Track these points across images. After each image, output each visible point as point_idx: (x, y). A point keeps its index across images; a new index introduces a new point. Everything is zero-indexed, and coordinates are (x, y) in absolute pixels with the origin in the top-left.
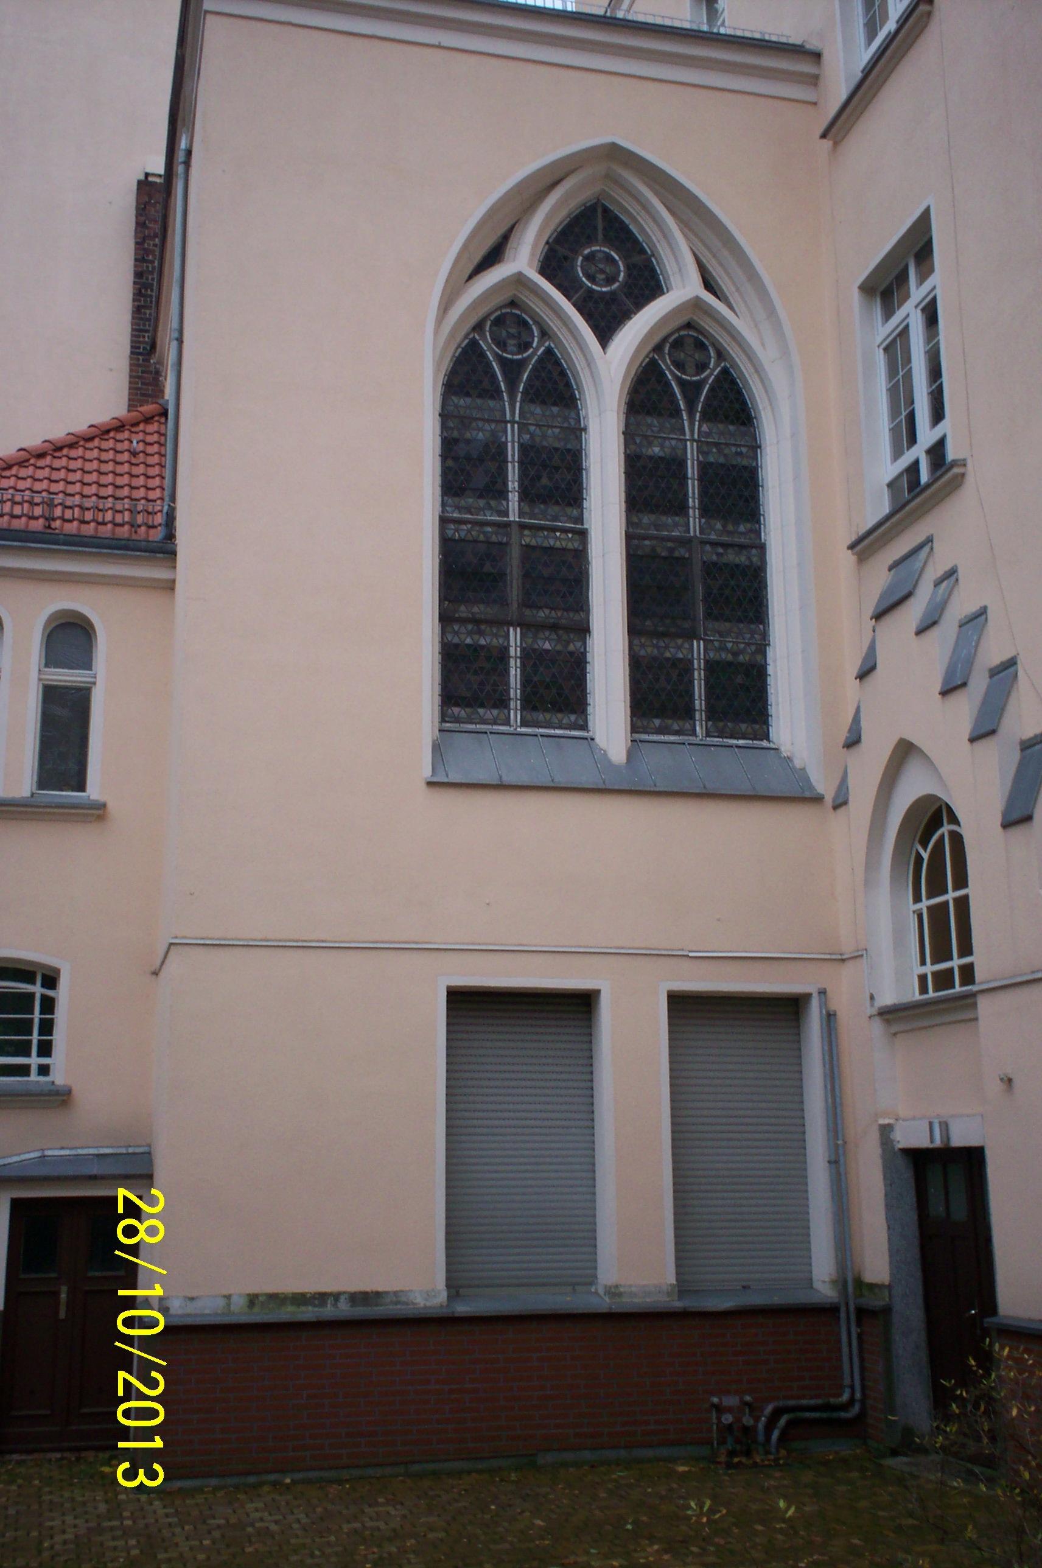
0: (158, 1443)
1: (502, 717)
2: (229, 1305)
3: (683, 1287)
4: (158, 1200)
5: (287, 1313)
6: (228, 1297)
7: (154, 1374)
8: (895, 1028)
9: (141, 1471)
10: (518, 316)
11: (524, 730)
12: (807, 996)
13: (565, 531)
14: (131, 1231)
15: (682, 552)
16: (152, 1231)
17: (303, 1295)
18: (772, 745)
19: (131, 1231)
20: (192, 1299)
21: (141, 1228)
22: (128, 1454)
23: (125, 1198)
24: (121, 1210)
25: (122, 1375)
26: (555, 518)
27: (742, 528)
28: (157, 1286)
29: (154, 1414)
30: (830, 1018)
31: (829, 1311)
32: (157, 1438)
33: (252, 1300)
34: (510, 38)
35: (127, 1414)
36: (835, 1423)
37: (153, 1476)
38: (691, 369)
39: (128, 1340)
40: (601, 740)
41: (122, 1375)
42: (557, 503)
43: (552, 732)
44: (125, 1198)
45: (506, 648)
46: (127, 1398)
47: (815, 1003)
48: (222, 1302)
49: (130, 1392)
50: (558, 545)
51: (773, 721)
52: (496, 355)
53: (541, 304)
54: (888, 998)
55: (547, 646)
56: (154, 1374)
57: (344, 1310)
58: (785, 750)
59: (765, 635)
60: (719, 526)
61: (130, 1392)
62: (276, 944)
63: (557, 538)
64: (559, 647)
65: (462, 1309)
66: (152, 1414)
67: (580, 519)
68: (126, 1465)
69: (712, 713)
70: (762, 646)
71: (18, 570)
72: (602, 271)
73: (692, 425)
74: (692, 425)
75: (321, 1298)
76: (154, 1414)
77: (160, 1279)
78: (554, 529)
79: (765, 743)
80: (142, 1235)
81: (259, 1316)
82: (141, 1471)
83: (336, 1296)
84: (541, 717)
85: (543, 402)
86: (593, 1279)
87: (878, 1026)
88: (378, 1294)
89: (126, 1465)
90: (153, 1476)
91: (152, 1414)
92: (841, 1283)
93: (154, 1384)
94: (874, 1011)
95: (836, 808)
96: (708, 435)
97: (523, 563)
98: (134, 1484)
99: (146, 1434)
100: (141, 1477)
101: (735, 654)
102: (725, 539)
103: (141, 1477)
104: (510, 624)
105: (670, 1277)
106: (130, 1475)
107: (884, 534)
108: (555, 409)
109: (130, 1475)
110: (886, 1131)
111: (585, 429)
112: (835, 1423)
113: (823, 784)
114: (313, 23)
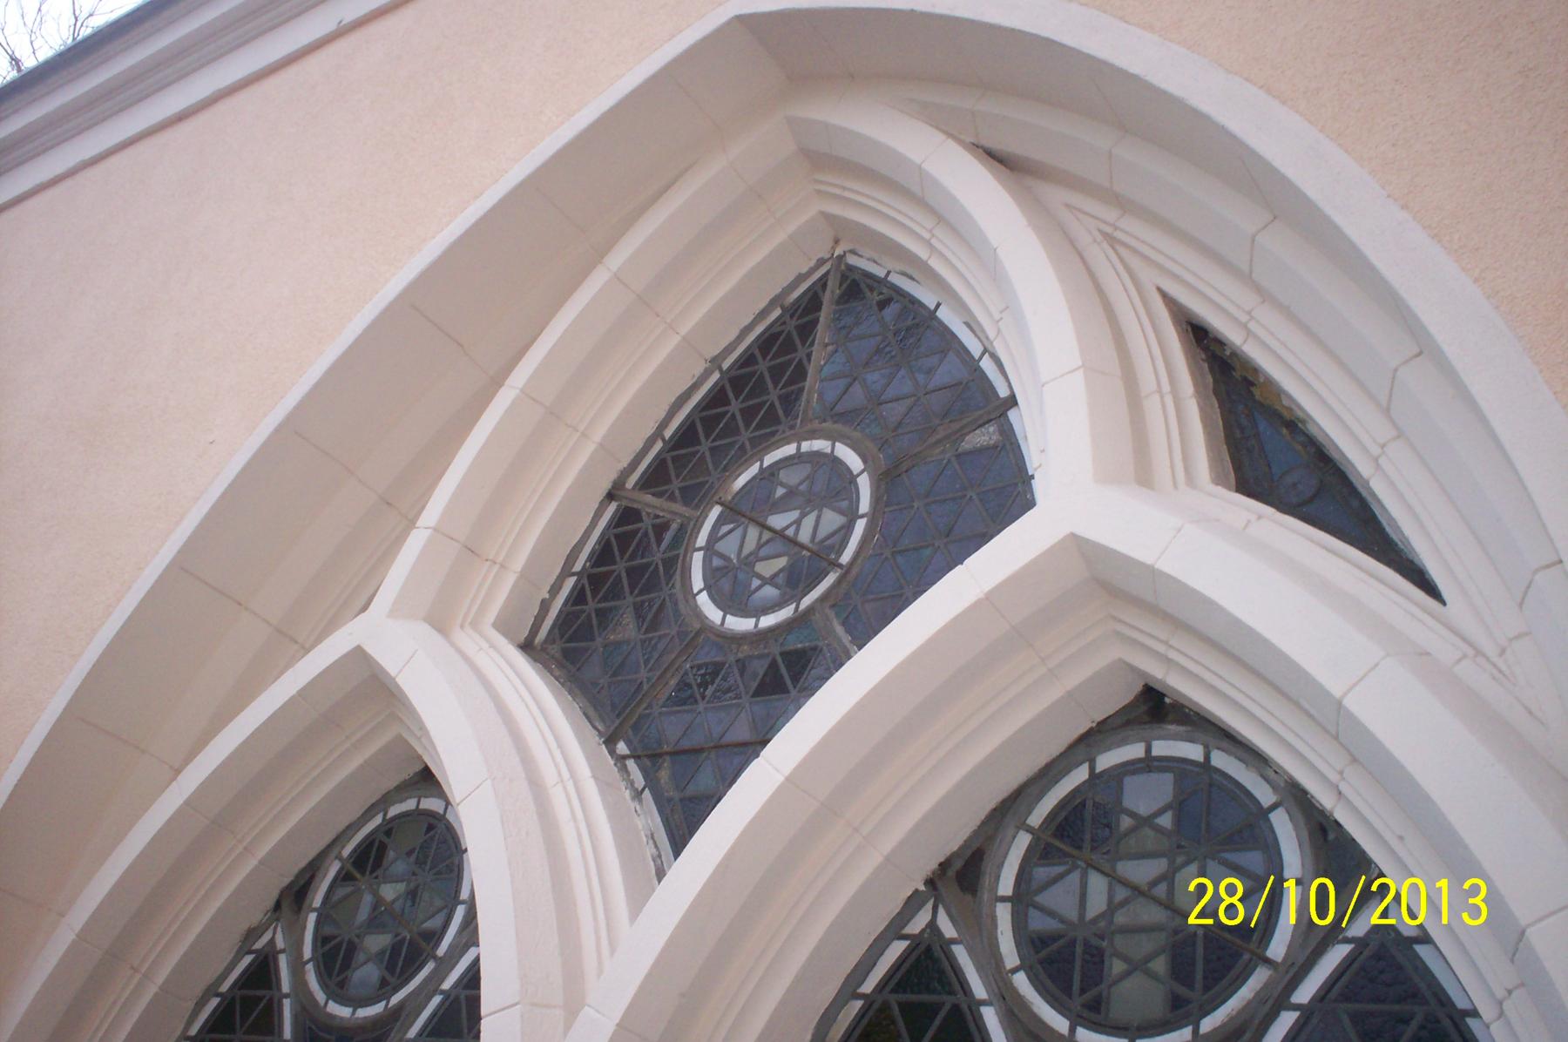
0: (1443, 884)
7: (1374, 888)
9: (1471, 901)
14: (1231, 909)
16: (1231, 890)
19: (1231, 909)
21: (1228, 900)
22: (1455, 913)
23: (1198, 917)
24: (1210, 921)
32: (1438, 885)
37: (1475, 890)
41: (1192, 920)
44: (1198, 917)
46: (1215, 915)
56: (1374, 888)
62: (557, 753)
68: (1465, 916)
80: (1234, 900)
82: (1471, 901)
89: (1465, 916)
90: (1475, 890)
93: (1202, 889)
97: (771, 419)
98: (1240, 907)
106: (1475, 912)
109: (1475, 912)
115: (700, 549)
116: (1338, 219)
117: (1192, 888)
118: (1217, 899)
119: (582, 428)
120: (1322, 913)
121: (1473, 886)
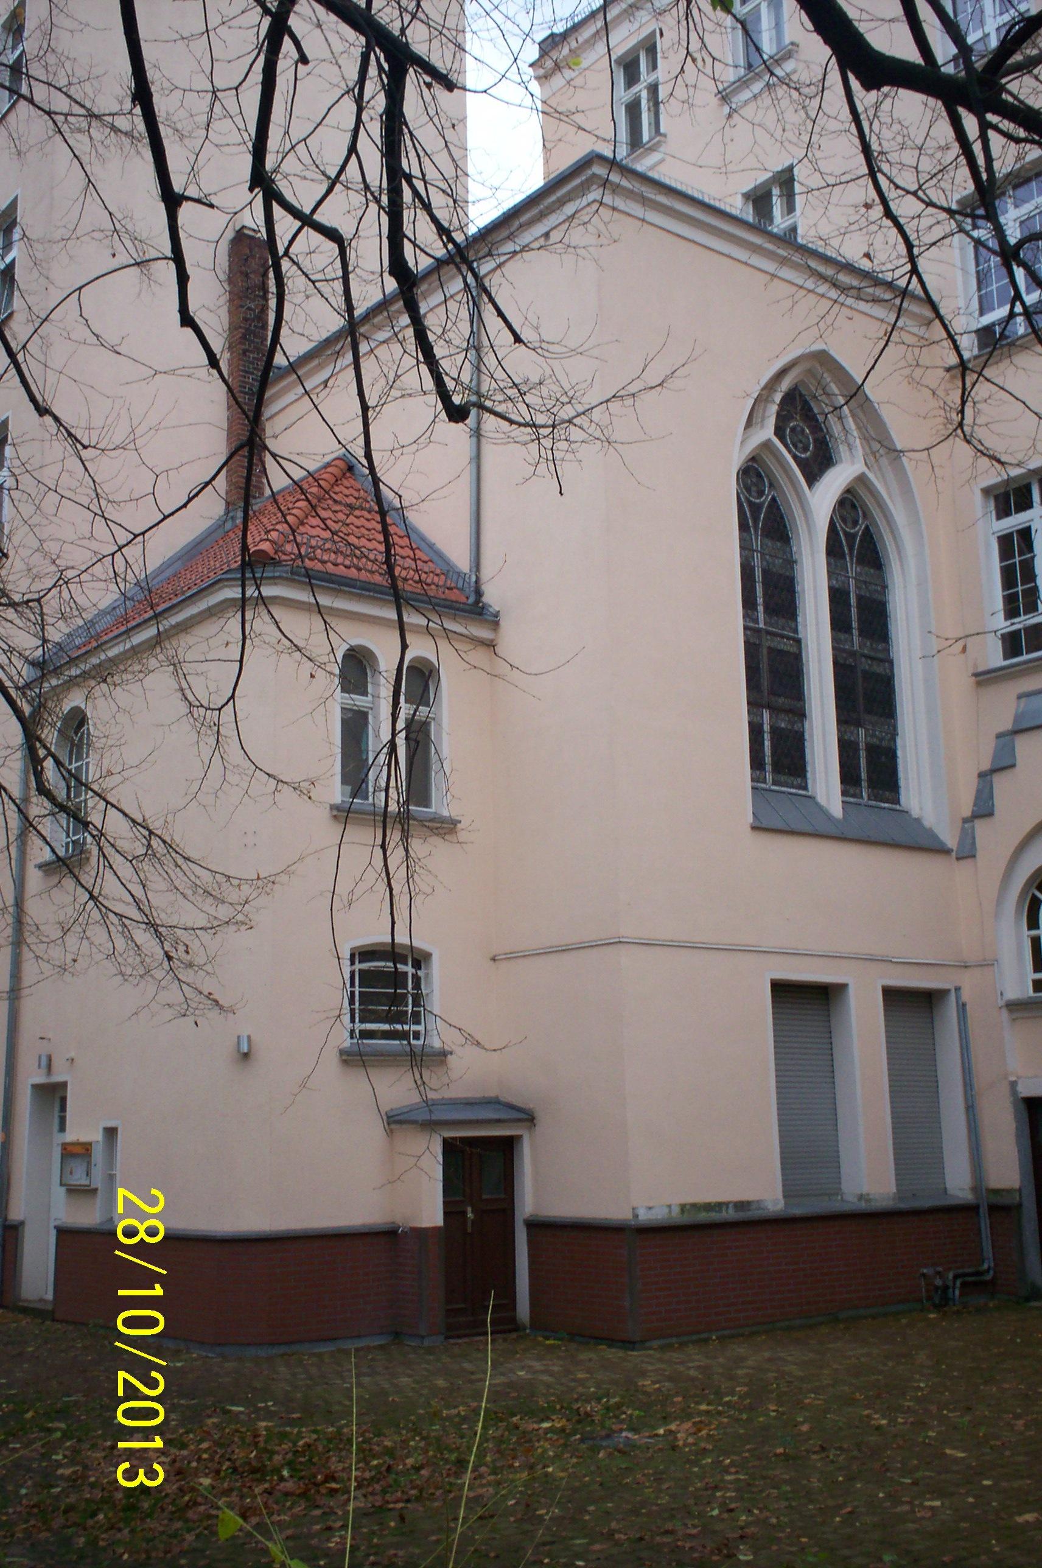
0: (158, 1443)
1: (762, 777)
2: (670, 1212)
3: (900, 1194)
4: (158, 1199)
5: (703, 1217)
6: (669, 1206)
7: (154, 1374)
8: (1015, 1015)
9: (141, 1471)
10: (757, 469)
11: (774, 788)
12: (948, 991)
13: (789, 638)
15: (850, 661)
16: (152, 1232)
17: (709, 1204)
18: (898, 807)
20: (650, 1208)
21: (142, 1228)
22: (130, 1454)
24: (121, 1393)
25: (122, 1375)
26: (783, 629)
27: (880, 647)
28: (157, 1286)
29: (154, 1414)
30: (962, 1008)
31: (968, 1210)
33: (683, 1207)
34: (678, 219)
35: (127, 1414)
36: (975, 1284)
38: (850, 525)
39: (128, 1340)
40: (821, 799)
41: (122, 1375)
42: (783, 617)
43: (790, 790)
45: (762, 725)
46: (126, 1398)
47: (953, 997)
48: (666, 1210)
49: (132, 1393)
50: (785, 649)
51: (902, 791)
52: (747, 499)
53: (774, 461)
54: (1012, 994)
55: (783, 725)
56: (154, 1374)
57: (730, 1215)
58: (915, 813)
59: (895, 728)
60: (868, 644)
61: (132, 1393)
63: (785, 644)
64: (789, 727)
65: (798, 1211)
66: (152, 1414)
67: (796, 631)
68: (126, 1465)
69: (872, 784)
70: (894, 734)
71: (365, 615)
72: (801, 442)
73: (757, 539)
74: (757, 539)
75: (719, 1206)
76: (154, 1414)
77: (158, 1278)
78: (782, 636)
79: (898, 807)
80: (142, 1235)
81: (686, 1219)
82: (141, 1471)
83: (727, 1204)
84: (783, 778)
85: (772, 538)
86: (838, 1191)
87: (1005, 1014)
88: (749, 1203)
89: (126, 1465)
90: (151, 1474)
91: (152, 1414)
92: (975, 1189)
93: (153, 1384)
94: (1001, 1003)
95: (958, 859)
96: (861, 574)
99: (147, 1434)
100: (141, 1478)
101: (881, 740)
102: (872, 654)
103: (141, 1478)
104: (763, 707)
105: (893, 1189)
106: (130, 1475)
107: (1011, 673)
108: (779, 544)
109: (130, 1475)
110: (1013, 1085)
111: (796, 562)
112: (975, 1284)
113: (950, 840)
114: (708, 244)
115: (395, 967)
116: (1017, 1167)
117: (154, 1191)
118: (143, 1216)
119: (159, 609)
120: (129, 1323)
121: (157, 1473)
